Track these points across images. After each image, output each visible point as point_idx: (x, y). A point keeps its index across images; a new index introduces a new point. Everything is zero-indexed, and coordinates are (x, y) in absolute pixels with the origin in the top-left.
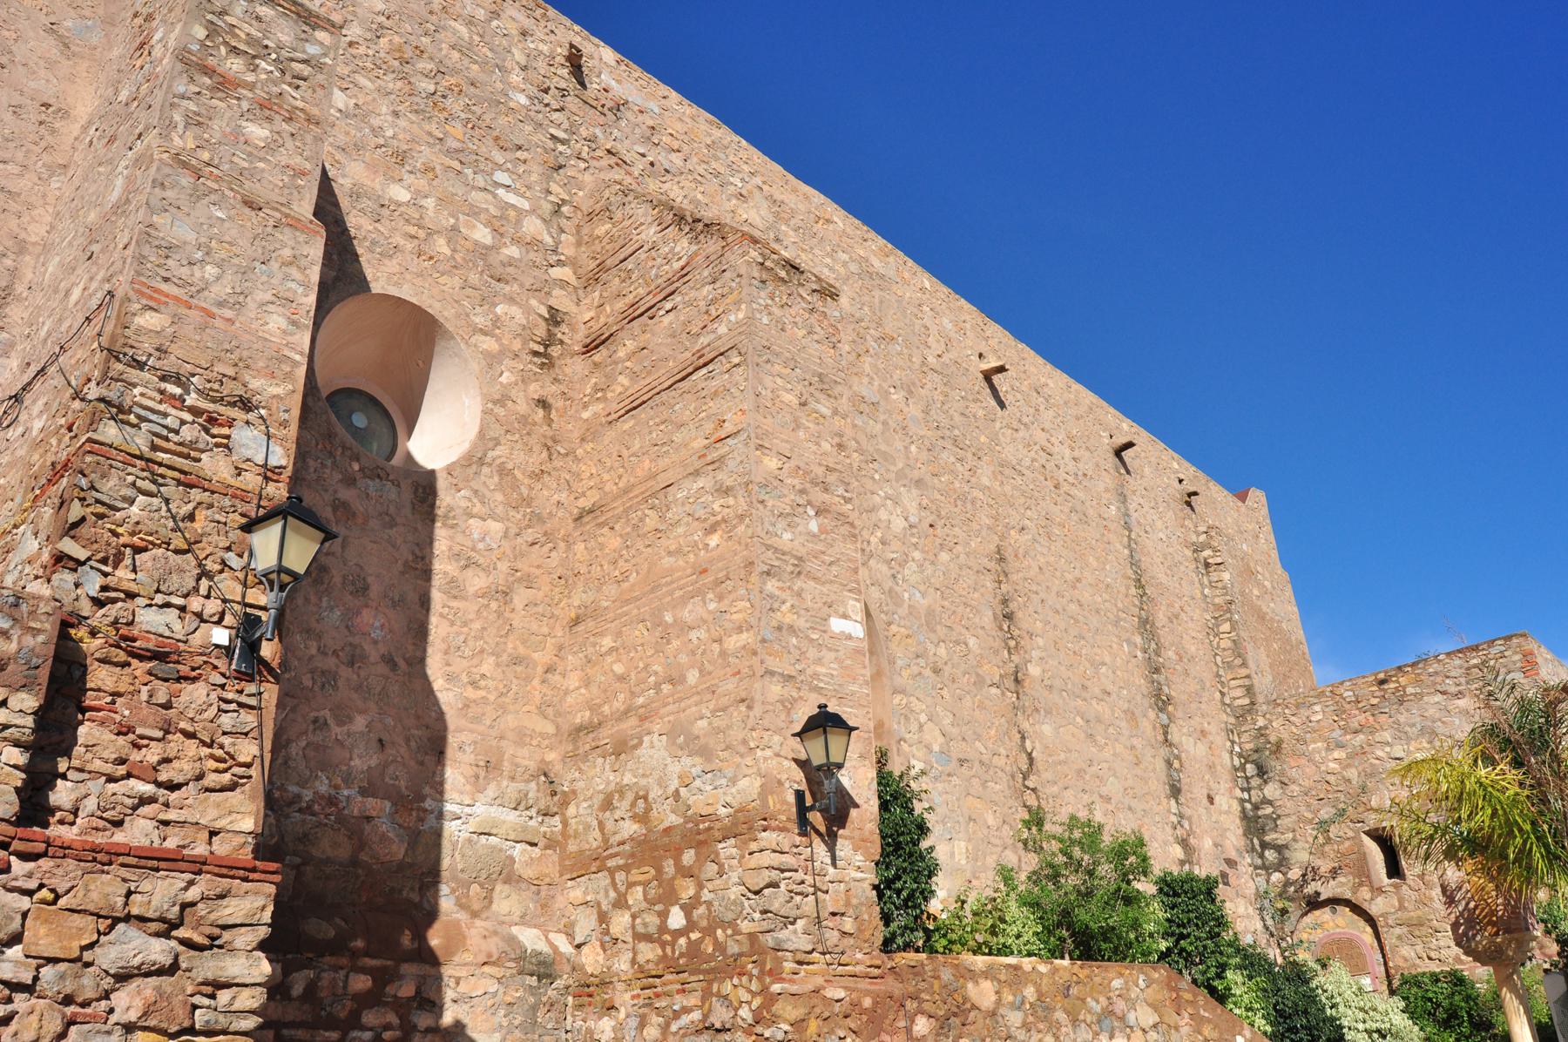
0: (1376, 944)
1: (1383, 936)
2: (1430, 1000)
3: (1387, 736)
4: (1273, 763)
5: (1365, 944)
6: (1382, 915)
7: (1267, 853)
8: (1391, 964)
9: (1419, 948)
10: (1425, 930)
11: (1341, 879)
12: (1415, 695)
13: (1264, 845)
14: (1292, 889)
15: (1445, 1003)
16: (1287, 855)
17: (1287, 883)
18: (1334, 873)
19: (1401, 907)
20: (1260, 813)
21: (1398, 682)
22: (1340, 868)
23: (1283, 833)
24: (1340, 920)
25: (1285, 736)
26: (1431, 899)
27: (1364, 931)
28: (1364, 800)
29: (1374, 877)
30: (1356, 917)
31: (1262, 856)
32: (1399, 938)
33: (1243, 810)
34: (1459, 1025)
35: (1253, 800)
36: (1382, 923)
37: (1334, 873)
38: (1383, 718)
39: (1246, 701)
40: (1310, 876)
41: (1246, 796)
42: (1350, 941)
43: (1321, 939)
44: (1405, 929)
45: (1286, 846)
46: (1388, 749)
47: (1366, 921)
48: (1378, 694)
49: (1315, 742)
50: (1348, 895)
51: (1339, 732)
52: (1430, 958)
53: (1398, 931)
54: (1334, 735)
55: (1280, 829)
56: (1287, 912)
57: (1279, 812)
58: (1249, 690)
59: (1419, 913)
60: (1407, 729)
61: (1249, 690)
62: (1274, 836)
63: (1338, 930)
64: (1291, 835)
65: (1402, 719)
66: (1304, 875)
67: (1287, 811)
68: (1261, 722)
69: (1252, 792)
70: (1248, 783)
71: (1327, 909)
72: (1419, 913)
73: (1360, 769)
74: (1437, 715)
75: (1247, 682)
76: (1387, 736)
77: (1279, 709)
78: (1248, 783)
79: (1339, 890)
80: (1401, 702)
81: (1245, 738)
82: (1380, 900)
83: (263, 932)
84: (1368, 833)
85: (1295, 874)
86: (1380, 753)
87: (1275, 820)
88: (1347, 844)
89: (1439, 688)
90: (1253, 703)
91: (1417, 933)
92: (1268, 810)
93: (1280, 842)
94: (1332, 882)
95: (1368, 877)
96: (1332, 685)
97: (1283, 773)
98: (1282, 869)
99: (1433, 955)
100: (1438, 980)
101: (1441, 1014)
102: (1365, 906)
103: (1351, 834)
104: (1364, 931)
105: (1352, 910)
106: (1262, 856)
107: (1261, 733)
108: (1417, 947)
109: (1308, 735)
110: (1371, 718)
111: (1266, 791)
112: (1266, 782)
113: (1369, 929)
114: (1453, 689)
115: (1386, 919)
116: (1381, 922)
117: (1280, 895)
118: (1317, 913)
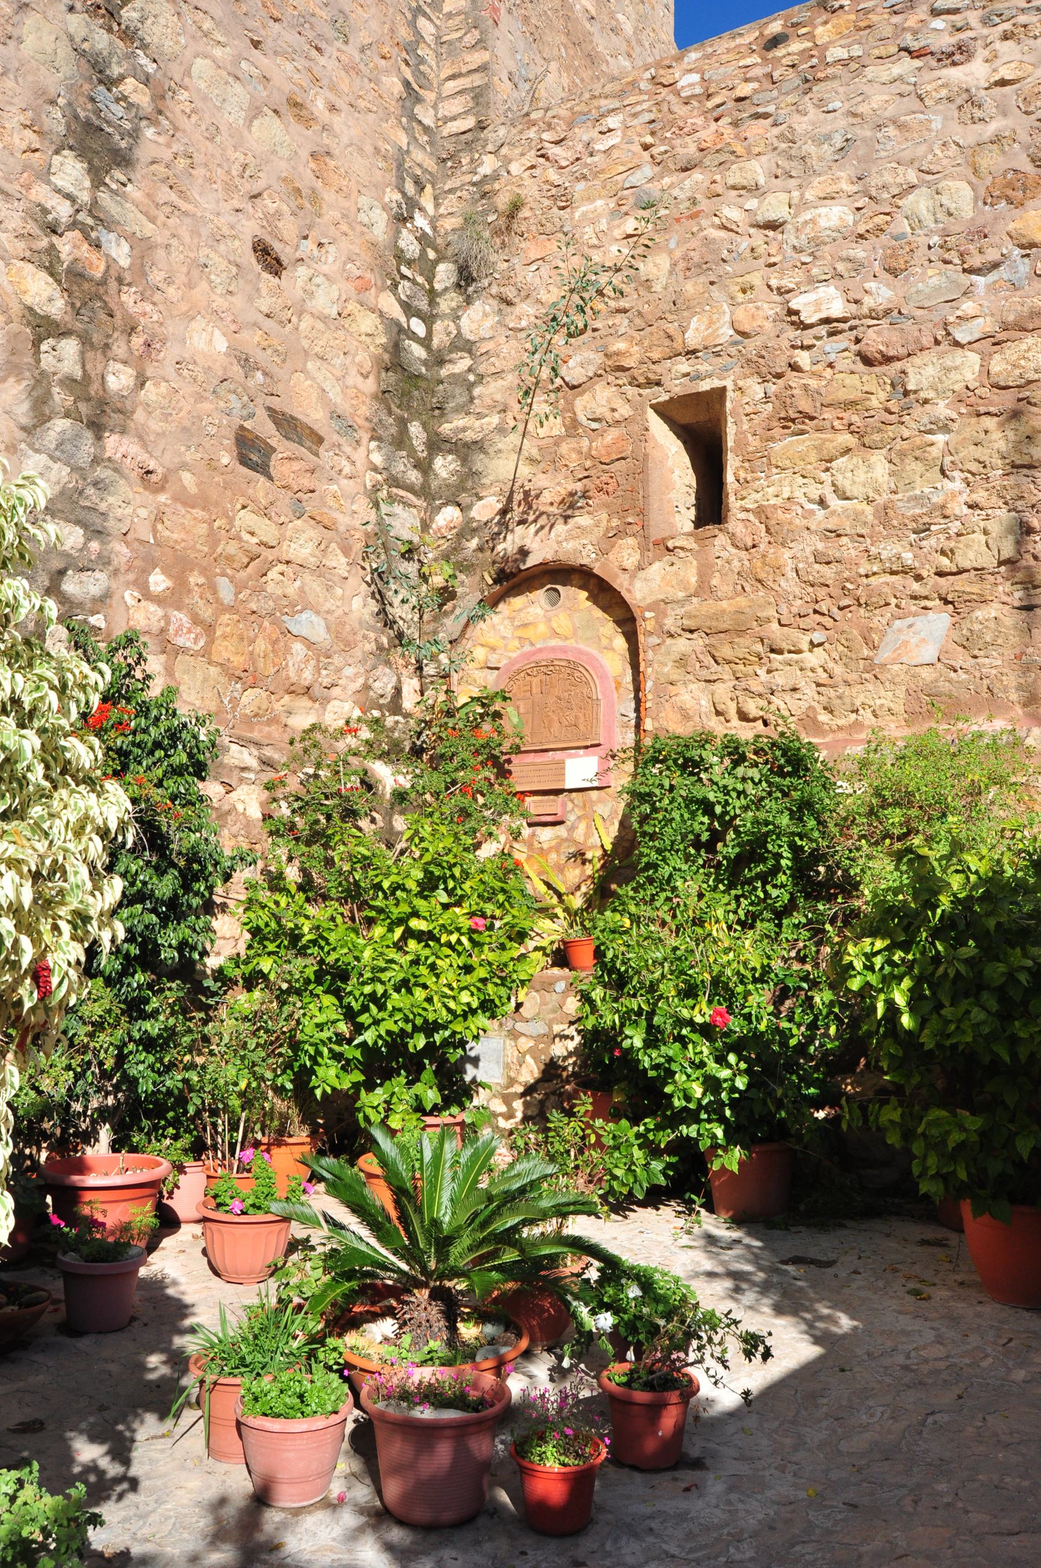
0: (629, 678)
1: (646, 655)
2: (707, 807)
3: (757, 170)
4: (493, 258)
5: (603, 676)
6: (649, 608)
7: (439, 462)
8: (648, 724)
9: (722, 691)
10: (747, 645)
11: (583, 520)
12: (844, 63)
13: (436, 444)
14: (474, 543)
15: (746, 821)
16: (478, 466)
17: (467, 530)
18: (570, 506)
19: (704, 589)
20: (444, 372)
21: (811, 36)
22: (585, 495)
23: (480, 416)
24: (562, 621)
25: (530, 190)
26: (778, 569)
27: (610, 648)
28: (672, 328)
29: (655, 517)
30: (598, 613)
31: (424, 467)
32: (682, 662)
33: (396, 349)
34: (765, 878)
35: (436, 343)
36: (650, 626)
37: (570, 506)
38: (756, 129)
39: (470, 122)
40: (516, 514)
41: (418, 327)
42: (573, 666)
43: (512, 662)
44: (699, 642)
45: (479, 446)
46: (752, 204)
47: (618, 623)
48: (758, 72)
49: (590, 199)
50: (587, 557)
51: (648, 171)
52: (743, 716)
53: (682, 645)
54: (637, 178)
55: (477, 406)
56: (453, 596)
57: (481, 369)
58: (479, 96)
59: (742, 601)
60: (810, 148)
61: (479, 96)
62: (460, 421)
63: (554, 642)
64: (495, 420)
65: (801, 125)
66: (504, 512)
67: (499, 364)
68: (488, 165)
69: (438, 326)
70: (432, 303)
71: (540, 595)
72: (742, 601)
73: (678, 254)
74: (890, 111)
75: (477, 80)
76: (757, 170)
77: (532, 133)
78: (432, 303)
79: (569, 546)
80: (808, 83)
81: (450, 203)
82: (657, 569)
83: (339, 1087)
84: (661, 410)
85: (485, 509)
86: (732, 213)
87: (470, 386)
88: (612, 435)
89: (909, 40)
90: (481, 126)
91: (726, 652)
92: (461, 364)
93: (469, 436)
94: (560, 528)
95: (642, 513)
96: (658, 65)
97: (508, 279)
98: (464, 498)
99: (752, 707)
100: (739, 759)
101: (728, 849)
102: (620, 583)
103: (625, 411)
104: (610, 648)
105: (593, 598)
106: (424, 467)
107: (484, 190)
108: (719, 687)
109: (581, 186)
110: (728, 132)
111: (464, 322)
112: (469, 301)
113: (620, 643)
114: (945, 41)
115: (660, 615)
116: (647, 622)
117: (446, 557)
118: (518, 602)
